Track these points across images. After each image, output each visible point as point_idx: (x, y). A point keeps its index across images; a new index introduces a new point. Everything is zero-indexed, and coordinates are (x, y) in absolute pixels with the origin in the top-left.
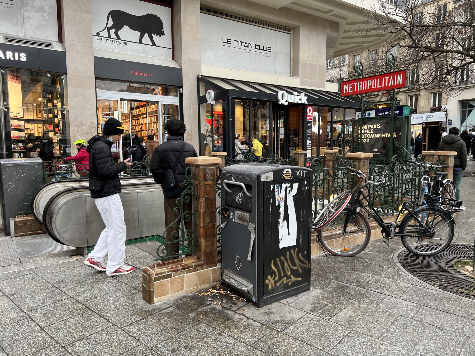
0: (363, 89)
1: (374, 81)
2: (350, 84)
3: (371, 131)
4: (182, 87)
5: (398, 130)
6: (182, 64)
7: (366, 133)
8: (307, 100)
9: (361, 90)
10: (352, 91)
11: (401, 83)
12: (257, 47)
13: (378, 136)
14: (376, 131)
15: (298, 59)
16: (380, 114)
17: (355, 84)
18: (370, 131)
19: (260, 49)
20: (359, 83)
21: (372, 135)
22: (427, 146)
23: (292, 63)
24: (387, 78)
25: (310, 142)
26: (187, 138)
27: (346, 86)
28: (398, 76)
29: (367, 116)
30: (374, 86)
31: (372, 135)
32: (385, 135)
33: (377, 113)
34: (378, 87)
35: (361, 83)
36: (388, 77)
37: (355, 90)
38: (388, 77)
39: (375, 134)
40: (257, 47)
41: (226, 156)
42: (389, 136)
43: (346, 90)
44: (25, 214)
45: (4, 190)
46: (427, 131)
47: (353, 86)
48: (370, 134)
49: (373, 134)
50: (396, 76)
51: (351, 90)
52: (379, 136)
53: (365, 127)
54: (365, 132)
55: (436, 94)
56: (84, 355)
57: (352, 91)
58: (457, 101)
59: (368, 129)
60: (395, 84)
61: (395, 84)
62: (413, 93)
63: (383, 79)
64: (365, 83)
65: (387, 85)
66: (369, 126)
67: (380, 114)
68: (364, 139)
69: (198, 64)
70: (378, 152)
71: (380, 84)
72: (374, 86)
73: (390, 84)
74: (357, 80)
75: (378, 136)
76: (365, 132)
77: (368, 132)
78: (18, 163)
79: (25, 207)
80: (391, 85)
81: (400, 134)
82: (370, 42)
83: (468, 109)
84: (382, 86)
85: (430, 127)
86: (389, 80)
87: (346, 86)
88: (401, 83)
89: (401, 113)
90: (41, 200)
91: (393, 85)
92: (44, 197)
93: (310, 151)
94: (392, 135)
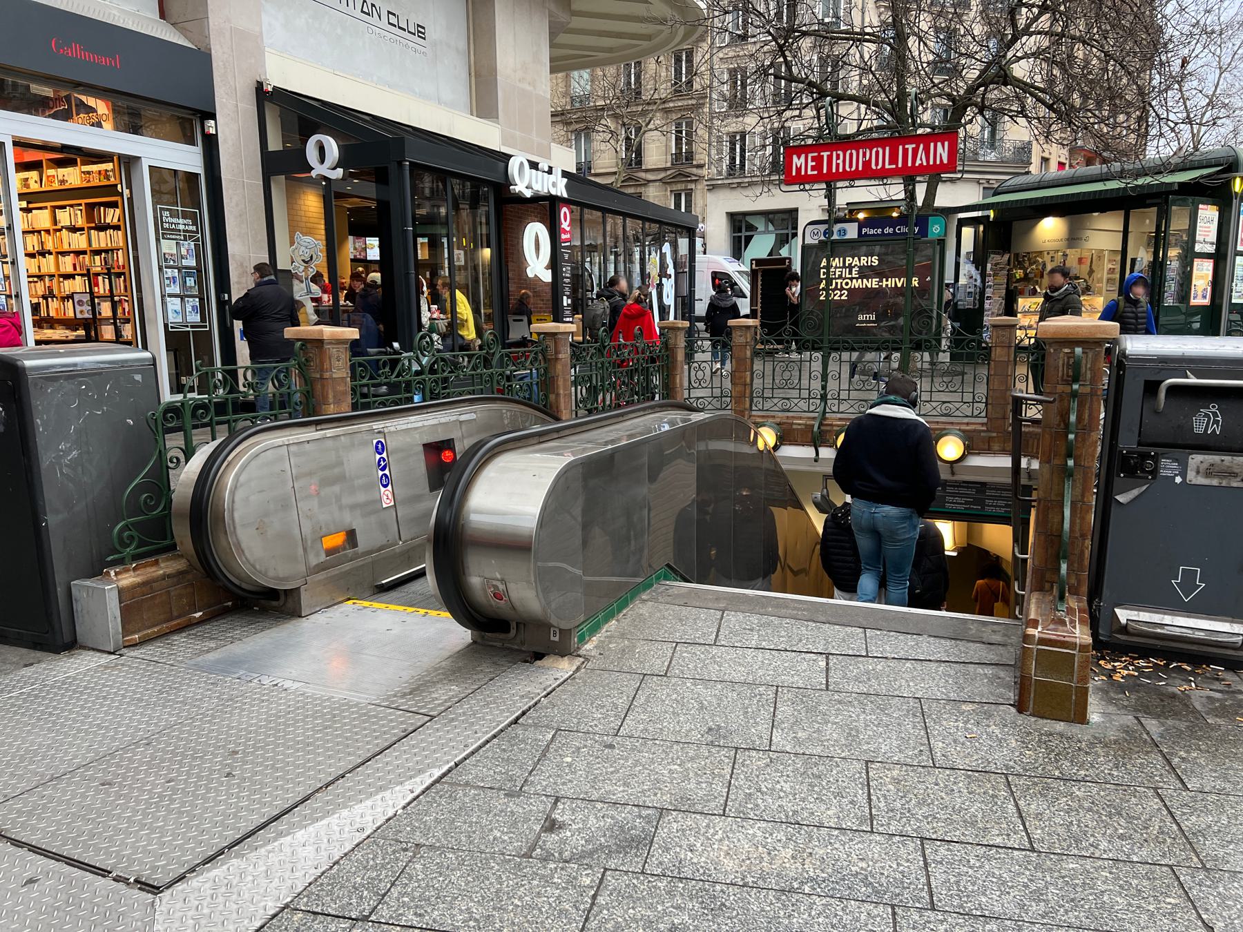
0: (848, 169)
1: (877, 153)
2: (810, 156)
3: (854, 272)
4: (213, 116)
5: (923, 272)
6: (208, 37)
7: (840, 277)
9: (841, 170)
10: (816, 172)
11: (945, 161)
12: (393, 20)
13: (873, 283)
14: (864, 273)
15: (493, 71)
16: (872, 232)
17: (825, 154)
18: (850, 273)
19: (400, 28)
20: (834, 153)
21: (854, 281)
23: (473, 78)
24: (910, 147)
25: (569, 301)
26: (238, 283)
27: (799, 159)
28: (939, 144)
29: (835, 237)
30: (877, 164)
31: (854, 281)
32: (889, 283)
34: (887, 166)
35: (841, 153)
36: (914, 146)
37: (825, 171)
38: (914, 146)
39: (865, 280)
40: (393, 20)
41: (354, 344)
42: (899, 285)
43: (799, 170)
44: (135, 558)
45: (43, 472)
46: (760, 278)
47: (818, 160)
48: (851, 279)
49: (860, 281)
50: (932, 145)
51: (813, 168)
53: (836, 262)
54: (837, 273)
56: (942, 928)
57: (816, 172)
59: (844, 266)
60: (931, 163)
61: (931, 163)
62: (682, 186)
63: (901, 147)
64: (851, 155)
65: (910, 164)
66: (849, 260)
67: (872, 232)
68: (833, 290)
69: (252, 45)
71: (893, 160)
72: (877, 164)
73: (918, 162)
74: (830, 147)
75: (873, 283)
76: (837, 273)
77: (846, 273)
78: (83, 363)
79: (134, 533)
80: (921, 165)
82: (610, 50)
83: (744, 234)
84: (897, 165)
86: (915, 151)
87: (799, 159)
88: (945, 161)
89: (924, 232)
90: (237, 499)
91: (925, 164)
92: (241, 486)
94: (909, 282)
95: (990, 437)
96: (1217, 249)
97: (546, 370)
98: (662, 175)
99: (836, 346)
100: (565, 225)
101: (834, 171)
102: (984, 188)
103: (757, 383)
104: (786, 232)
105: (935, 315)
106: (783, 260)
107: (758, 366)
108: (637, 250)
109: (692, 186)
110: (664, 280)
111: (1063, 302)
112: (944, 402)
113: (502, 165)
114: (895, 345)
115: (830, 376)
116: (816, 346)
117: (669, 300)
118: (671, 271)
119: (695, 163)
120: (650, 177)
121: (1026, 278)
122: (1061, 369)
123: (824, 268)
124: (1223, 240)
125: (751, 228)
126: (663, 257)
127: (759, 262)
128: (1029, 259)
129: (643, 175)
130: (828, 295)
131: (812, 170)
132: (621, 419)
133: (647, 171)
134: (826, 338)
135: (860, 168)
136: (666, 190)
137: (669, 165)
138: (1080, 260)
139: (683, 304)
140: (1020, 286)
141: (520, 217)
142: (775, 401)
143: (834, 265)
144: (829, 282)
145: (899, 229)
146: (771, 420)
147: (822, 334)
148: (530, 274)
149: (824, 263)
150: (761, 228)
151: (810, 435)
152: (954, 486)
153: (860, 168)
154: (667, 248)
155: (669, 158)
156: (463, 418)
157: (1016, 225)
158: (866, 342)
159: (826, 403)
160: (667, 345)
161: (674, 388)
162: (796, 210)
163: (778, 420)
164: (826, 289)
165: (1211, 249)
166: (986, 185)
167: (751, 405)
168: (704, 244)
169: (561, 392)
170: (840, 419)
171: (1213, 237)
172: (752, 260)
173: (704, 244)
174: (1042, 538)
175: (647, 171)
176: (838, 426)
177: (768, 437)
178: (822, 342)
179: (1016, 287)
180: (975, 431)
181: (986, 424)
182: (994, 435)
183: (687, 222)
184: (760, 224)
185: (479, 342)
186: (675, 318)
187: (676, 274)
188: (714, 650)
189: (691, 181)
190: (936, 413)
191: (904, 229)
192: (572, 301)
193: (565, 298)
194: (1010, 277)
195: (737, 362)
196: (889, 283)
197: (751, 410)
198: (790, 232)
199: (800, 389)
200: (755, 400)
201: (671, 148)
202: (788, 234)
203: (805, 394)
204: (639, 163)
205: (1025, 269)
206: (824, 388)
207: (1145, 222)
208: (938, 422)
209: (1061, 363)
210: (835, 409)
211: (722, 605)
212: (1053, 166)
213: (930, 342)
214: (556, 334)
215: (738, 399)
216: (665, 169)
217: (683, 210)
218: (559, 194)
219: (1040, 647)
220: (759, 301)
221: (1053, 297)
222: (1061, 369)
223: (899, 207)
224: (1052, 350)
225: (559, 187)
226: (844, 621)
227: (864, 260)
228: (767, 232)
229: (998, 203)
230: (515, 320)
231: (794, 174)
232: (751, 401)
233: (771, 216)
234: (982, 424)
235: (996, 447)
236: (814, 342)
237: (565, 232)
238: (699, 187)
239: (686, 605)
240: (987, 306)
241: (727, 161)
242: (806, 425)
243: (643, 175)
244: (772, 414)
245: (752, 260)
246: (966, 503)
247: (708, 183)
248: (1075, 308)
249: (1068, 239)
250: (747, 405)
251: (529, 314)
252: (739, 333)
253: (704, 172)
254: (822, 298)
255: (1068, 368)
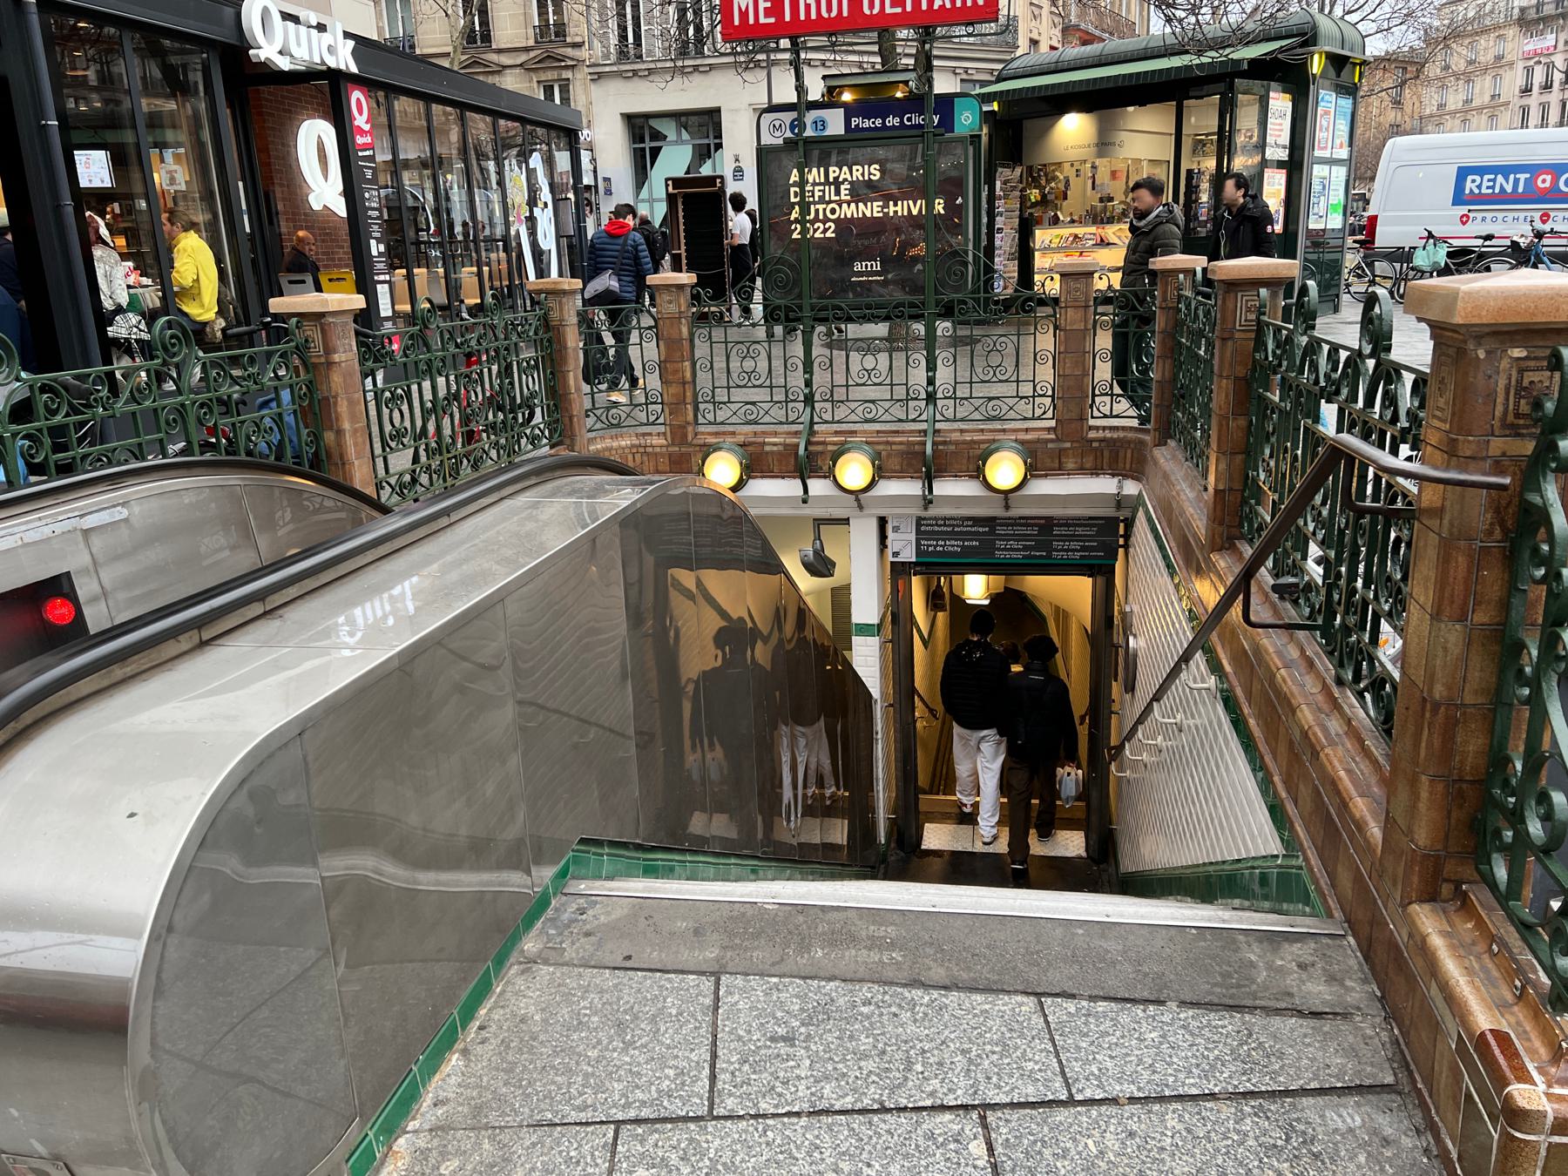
3: (843, 192)
8: (354, 53)
9: (813, 16)
10: (772, 20)
13: (873, 210)
14: (861, 192)
16: (867, 124)
18: (838, 193)
21: (845, 206)
22: (684, 261)
25: (382, 248)
29: (809, 133)
31: (845, 206)
33: (854, 122)
34: (888, 10)
37: (787, 18)
39: (861, 205)
42: (915, 212)
46: (680, 207)
52: (875, 209)
53: (814, 175)
54: (817, 194)
55: (552, 87)
57: (772, 20)
58: (619, 117)
59: (827, 182)
66: (833, 172)
67: (867, 124)
68: (813, 222)
70: (877, 273)
81: (959, 201)
83: (648, 145)
85: (686, 194)
89: (948, 122)
93: (386, 286)
94: (930, 206)
95: (1061, 450)
96: (1291, 155)
97: (311, 385)
98: (522, 58)
99: (823, 314)
100: (361, 121)
101: (802, 17)
102: (962, 80)
103: (703, 379)
104: (706, 141)
105: (970, 258)
106: (711, 180)
107: (701, 350)
108: (491, 166)
109: (567, 74)
110: (537, 211)
111: (1151, 237)
112: (990, 399)
113: (229, 11)
114: (914, 311)
115: (816, 365)
116: (792, 315)
117: (548, 242)
118: (545, 195)
119: (569, 40)
120: (505, 60)
121: (1044, 201)
122: (1500, 400)
123: (795, 184)
124: (1297, 142)
125: (657, 136)
126: (531, 174)
127: (677, 182)
128: (1046, 175)
129: (494, 57)
130: (804, 231)
131: (766, 16)
132: (444, 521)
133: (500, 51)
134: (806, 302)
135: (845, 14)
136: (531, 81)
137: (531, 42)
138: (1114, 174)
139: (570, 247)
140: (1037, 212)
141: (290, 111)
142: (734, 407)
143: (811, 180)
144: (805, 207)
145: (909, 119)
146: (729, 439)
147: (800, 296)
148: (316, 204)
149: (794, 176)
150: (672, 136)
151: (792, 461)
152: (1007, 525)
153: (845, 14)
154: (536, 161)
155: (531, 32)
156: (91, 521)
157: (1027, 124)
158: (869, 307)
159: (813, 408)
160: (546, 320)
161: (567, 394)
162: (718, 111)
163: (741, 439)
164: (801, 221)
165: (1283, 155)
166: (965, 77)
167: (696, 416)
168: (593, 160)
169: (346, 426)
170: (837, 433)
171: (1285, 139)
172: (667, 180)
173: (593, 160)
174: (1440, 787)
175: (500, 51)
176: (835, 444)
177: (722, 471)
178: (801, 310)
179: (1031, 214)
180: (1038, 441)
181: (1054, 429)
182: (1068, 445)
183: (564, 120)
184: (669, 129)
185: (221, 323)
186: (561, 275)
187: (556, 201)
188: (715, 1139)
189: (567, 67)
190: (978, 417)
191: (917, 120)
192: (388, 248)
193: (373, 243)
194: (1023, 199)
195: (668, 347)
196: (900, 209)
197: (696, 423)
198: (712, 141)
199: (771, 387)
200: (702, 406)
201: (532, 18)
202: (709, 145)
203: (779, 396)
204: (487, 37)
205: (1041, 188)
206: (808, 384)
207: (1203, 118)
208: (982, 430)
209: (1502, 383)
210: (828, 417)
211: (709, 954)
212: (1044, 47)
213: (965, 303)
214: (322, 315)
215: (675, 407)
216: (527, 49)
217: (557, 101)
218: (343, 67)
219: (1556, 1139)
220: (683, 241)
221: (1139, 228)
222: (1500, 400)
223: (906, 83)
224: (1481, 354)
225: (344, 59)
226: (986, 974)
227: (858, 172)
228: (679, 142)
229: (1002, 92)
230: (291, 282)
231: (737, 22)
232: (696, 409)
233: (683, 119)
234: (1049, 429)
235: (1070, 464)
236: (788, 309)
237: (362, 132)
238: (579, 76)
239: (626, 966)
240: (997, 243)
241: (614, 40)
242: (785, 445)
243: (494, 57)
244: (731, 428)
245: (667, 180)
246: (1025, 548)
247: (591, 70)
248: (1166, 245)
249: (1097, 145)
250: (690, 417)
251: (315, 270)
252: (666, 297)
253: (583, 54)
254: (795, 236)
255: (1518, 396)
